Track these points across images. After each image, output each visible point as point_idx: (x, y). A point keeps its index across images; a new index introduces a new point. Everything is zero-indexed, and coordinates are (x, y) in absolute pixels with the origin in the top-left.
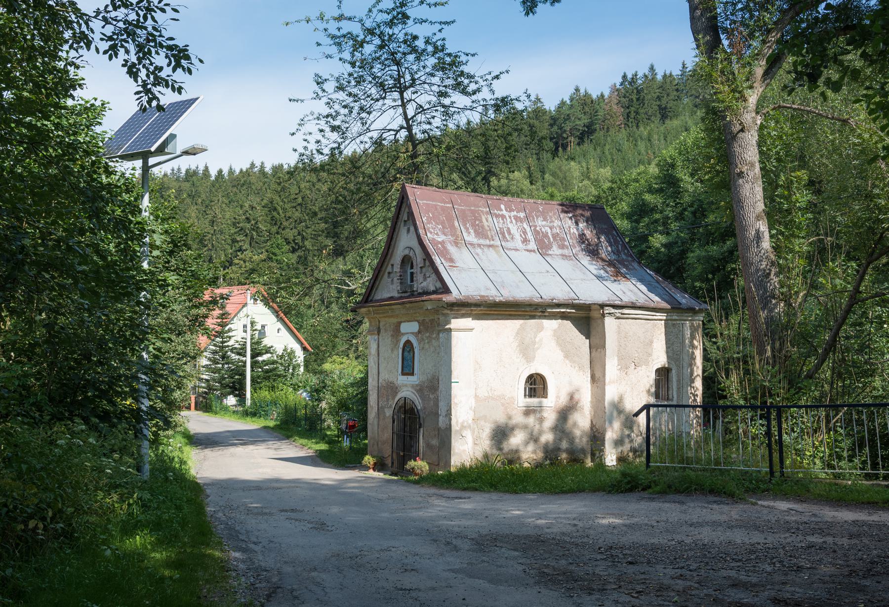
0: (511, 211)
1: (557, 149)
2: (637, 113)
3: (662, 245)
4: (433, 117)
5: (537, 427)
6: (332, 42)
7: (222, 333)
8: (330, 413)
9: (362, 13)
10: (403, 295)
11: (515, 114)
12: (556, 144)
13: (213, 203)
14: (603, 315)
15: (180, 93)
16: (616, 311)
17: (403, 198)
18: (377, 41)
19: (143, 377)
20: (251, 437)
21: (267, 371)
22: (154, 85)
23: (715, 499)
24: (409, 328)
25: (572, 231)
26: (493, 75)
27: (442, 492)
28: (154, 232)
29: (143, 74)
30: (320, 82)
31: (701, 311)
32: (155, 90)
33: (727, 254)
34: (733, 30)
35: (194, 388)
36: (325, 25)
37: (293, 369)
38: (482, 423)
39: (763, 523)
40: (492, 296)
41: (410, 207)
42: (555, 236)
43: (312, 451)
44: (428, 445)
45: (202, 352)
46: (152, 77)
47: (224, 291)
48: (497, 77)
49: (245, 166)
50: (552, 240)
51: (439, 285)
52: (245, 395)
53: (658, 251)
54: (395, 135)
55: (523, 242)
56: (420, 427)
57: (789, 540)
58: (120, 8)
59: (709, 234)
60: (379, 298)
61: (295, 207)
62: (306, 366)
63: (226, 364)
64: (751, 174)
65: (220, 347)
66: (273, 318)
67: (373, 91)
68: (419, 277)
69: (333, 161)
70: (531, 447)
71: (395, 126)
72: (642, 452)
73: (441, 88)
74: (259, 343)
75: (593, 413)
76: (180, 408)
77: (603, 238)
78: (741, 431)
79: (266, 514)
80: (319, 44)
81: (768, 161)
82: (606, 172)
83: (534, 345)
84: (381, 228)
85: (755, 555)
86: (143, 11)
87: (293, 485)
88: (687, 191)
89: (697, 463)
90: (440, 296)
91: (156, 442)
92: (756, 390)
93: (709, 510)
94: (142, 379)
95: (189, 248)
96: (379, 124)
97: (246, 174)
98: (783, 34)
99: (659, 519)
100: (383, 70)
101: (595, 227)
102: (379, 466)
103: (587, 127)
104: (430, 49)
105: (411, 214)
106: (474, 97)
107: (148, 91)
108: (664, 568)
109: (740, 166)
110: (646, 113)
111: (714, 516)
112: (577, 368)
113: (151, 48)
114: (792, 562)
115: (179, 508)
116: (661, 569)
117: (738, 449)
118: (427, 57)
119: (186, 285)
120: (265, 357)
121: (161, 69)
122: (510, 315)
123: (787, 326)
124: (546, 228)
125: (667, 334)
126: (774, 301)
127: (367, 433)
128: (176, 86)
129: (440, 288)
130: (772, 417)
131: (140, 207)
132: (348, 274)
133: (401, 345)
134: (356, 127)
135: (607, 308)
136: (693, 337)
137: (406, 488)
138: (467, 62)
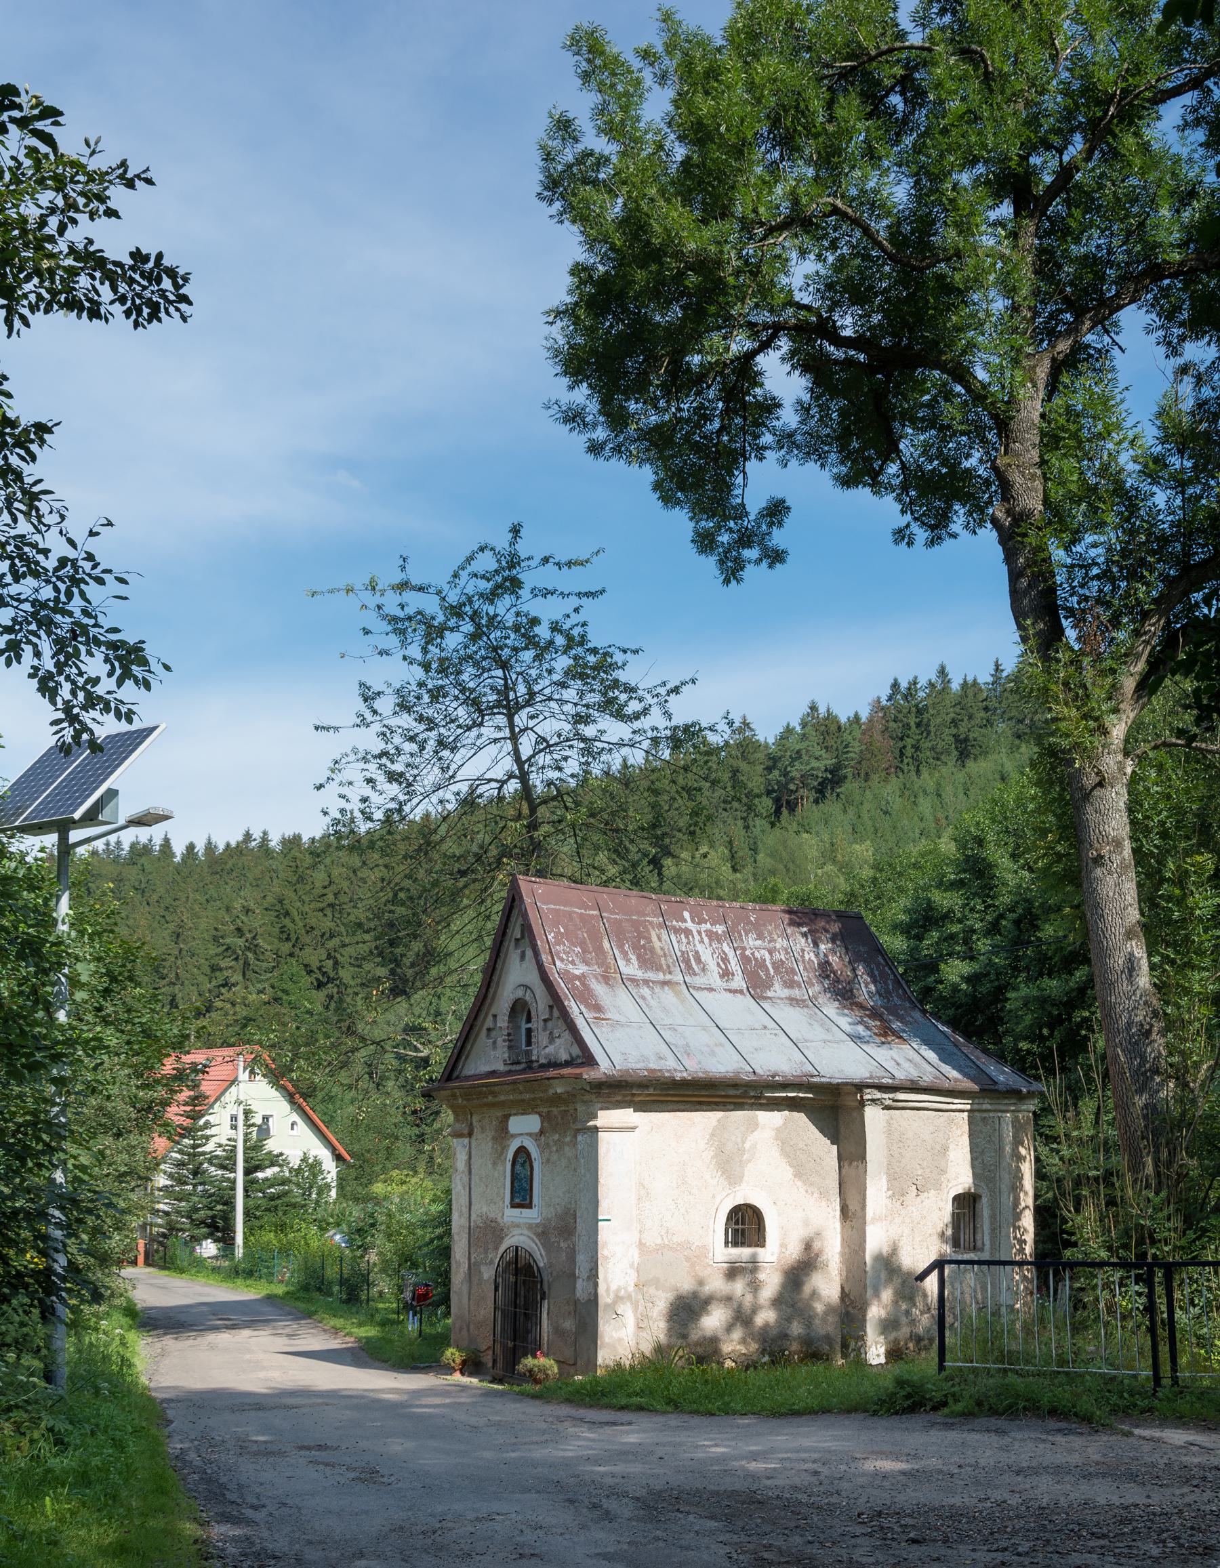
0: (704, 921)
1: (778, 812)
2: (917, 748)
3: (962, 977)
4: (566, 758)
5: (749, 1298)
6: (390, 628)
7: (193, 1130)
8: (383, 1271)
9: (441, 578)
10: (514, 1068)
11: (708, 753)
12: (777, 801)
13: (178, 903)
14: (862, 1104)
15: (130, 721)
16: (885, 1096)
17: (513, 899)
18: (468, 627)
19: (57, 1213)
20: (244, 1314)
21: (272, 1198)
22: (85, 708)
23: (1063, 1425)
24: (524, 1126)
25: (807, 957)
26: (670, 686)
27: (582, 1412)
28: (77, 959)
29: (65, 691)
30: (369, 697)
31: (1031, 1095)
32: (86, 717)
33: (1074, 994)
34: (1083, 611)
35: (143, 1227)
36: (378, 599)
37: (319, 1193)
38: (652, 1290)
39: (1143, 1470)
40: (668, 1071)
41: (525, 915)
42: (778, 966)
43: (352, 1339)
44: (558, 1331)
45: (158, 1164)
46: (81, 695)
47: (198, 1057)
48: (676, 690)
49: (235, 838)
50: (772, 972)
51: (576, 1051)
52: (233, 1239)
53: (955, 988)
54: (500, 789)
55: (722, 977)
56: (543, 1299)
57: (1188, 1500)
58: (24, 578)
59: (1043, 959)
60: (472, 1073)
61: (322, 910)
62: (341, 1187)
63: (201, 1184)
64: (1117, 860)
65: (189, 1154)
66: (285, 1106)
67: (461, 712)
68: (541, 1037)
69: (389, 833)
70: (737, 1334)
71: (499, 773)
72: (931, 1340)
73: (579, 708)
74: (258, 1147)
75: (844, 1273)
76: (120, 1263)
77: (861, 969)
78: (1102, 1305)
79: (272, 1453)
80: (367, 632)
81: (1145, 837)
82: (864, 851)
83: (743, 1154)
84: (472, 951)
85: (1130, 1527)
86: (64, 582)
87: (320, 1401)
88: (1005, 884)
89: (1027, 1362)
90: (578, 1071)
91: (77, 1325)
92: (1127, 1233)
93: (1049, 1446)
94: (53, 1217)
95: (138, 985)
96: (471, 770)
97: (238, 851)
98: (1169, 619)
99: (962, 1462)
100: (479, 676)
101: (847, 949)
102: (471, 1366)
103: (831, 772)
104: (560, 640)
105: (527, 930)
106: (637, 725)
107: (72, 719)
108: (974, 1550)
109: (1096, 845)
110: (932, 749)
111: (1059, 1456)
112: (816, 1195)
113: (80, 646)
114: (1195, 1539)
115: (119, 1445)
116: (968, 1552)
117: (1097, 1336)
118: (554, 656)
119: (131, 1049)
120: (269, 1172)
121: (96, 681)
122: (700, 1103)
123: (1181, 1121)
124: (763, 952)
125: (972, 1135)
126: (1158, 1079)
127: (449, 1307)
128: (124, 710)
129: (578, 1057)
130: (1157, 1280)
131: (55, 915)
132: (414, 1030)
133: (510, 1156)
134: (431, 775)
135: (868, 1091)
136: (1018, 1142)
137: (518, 1405)
138: (624, 664)
